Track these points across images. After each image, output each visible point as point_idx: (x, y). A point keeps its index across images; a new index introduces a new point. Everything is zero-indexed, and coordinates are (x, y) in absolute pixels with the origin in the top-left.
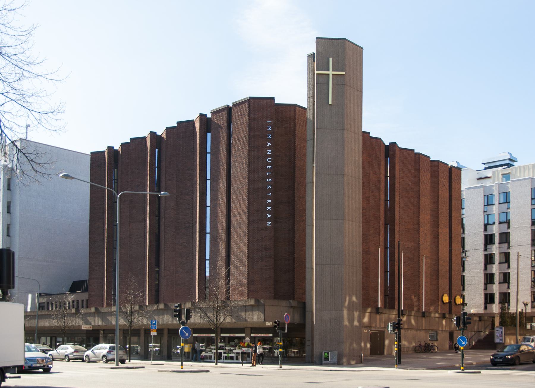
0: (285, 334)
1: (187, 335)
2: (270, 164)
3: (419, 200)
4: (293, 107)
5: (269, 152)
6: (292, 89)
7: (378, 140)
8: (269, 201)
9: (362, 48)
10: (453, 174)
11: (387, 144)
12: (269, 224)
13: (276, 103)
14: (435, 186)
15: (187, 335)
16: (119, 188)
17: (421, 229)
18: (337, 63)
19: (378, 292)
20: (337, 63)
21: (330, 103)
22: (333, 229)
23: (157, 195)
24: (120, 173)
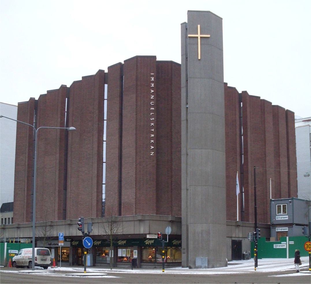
0: (167, 243)
1: (89, 244)
2: (153, 106)
3: (265, 135)
4: (171, 64)
5: (152, 97)
6: (170, 52)
7: (234, 89)
8: (153, 135)
9: (222, 19)
10: (289, 116)
11: (240, 92)
12: (152, 154)
13: (157, 60)
14: (276, 124)
15: (89, 244)
16: (38, 125)
17: (267, 158)
18: (203, 31)
19: (237, 209)
20: (203, 31)
21: (199, 58)
22: (203, 161)
23: (67, 129)
24: (38, 117)
